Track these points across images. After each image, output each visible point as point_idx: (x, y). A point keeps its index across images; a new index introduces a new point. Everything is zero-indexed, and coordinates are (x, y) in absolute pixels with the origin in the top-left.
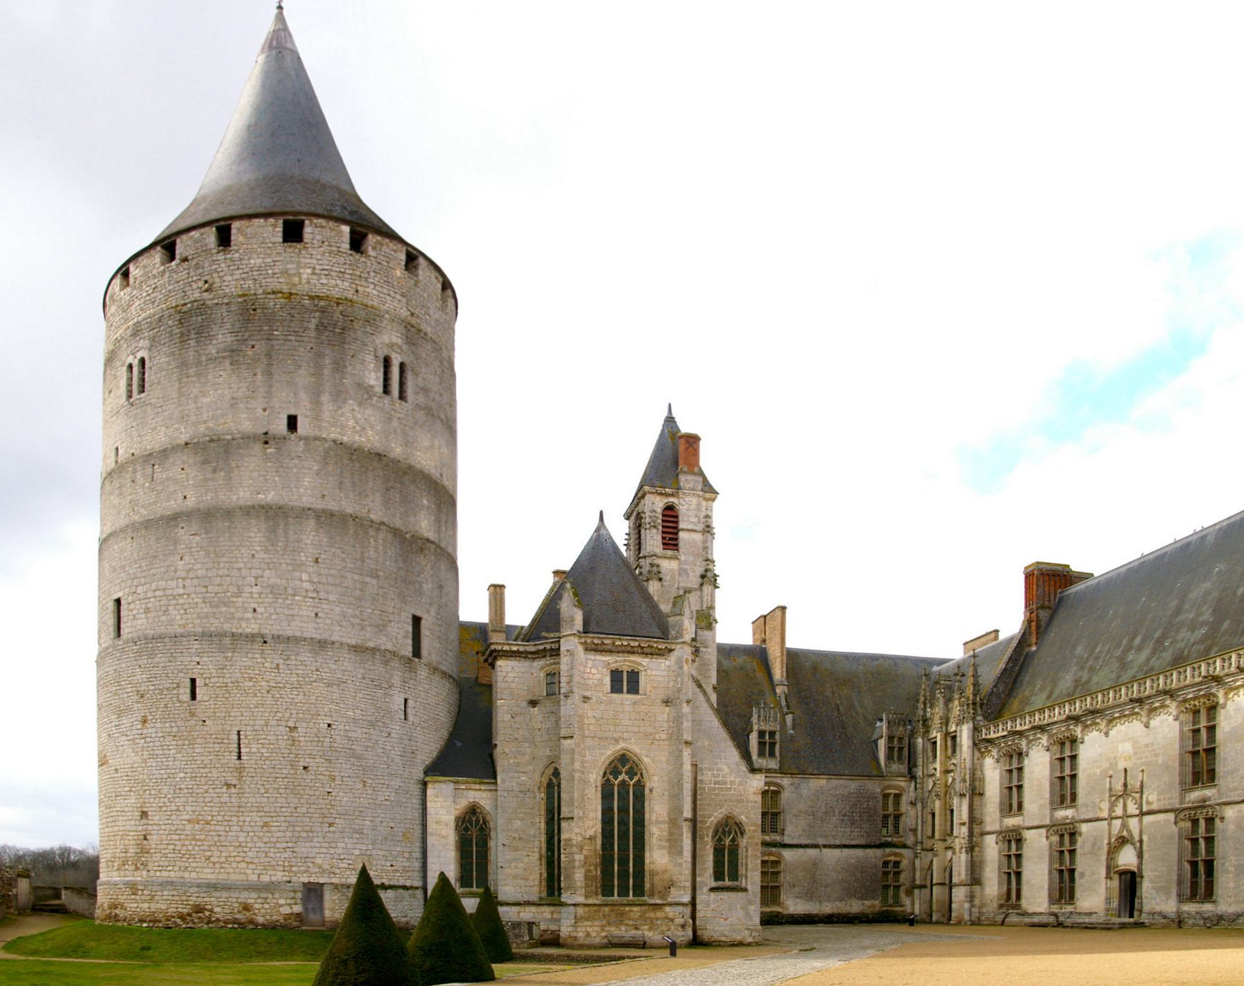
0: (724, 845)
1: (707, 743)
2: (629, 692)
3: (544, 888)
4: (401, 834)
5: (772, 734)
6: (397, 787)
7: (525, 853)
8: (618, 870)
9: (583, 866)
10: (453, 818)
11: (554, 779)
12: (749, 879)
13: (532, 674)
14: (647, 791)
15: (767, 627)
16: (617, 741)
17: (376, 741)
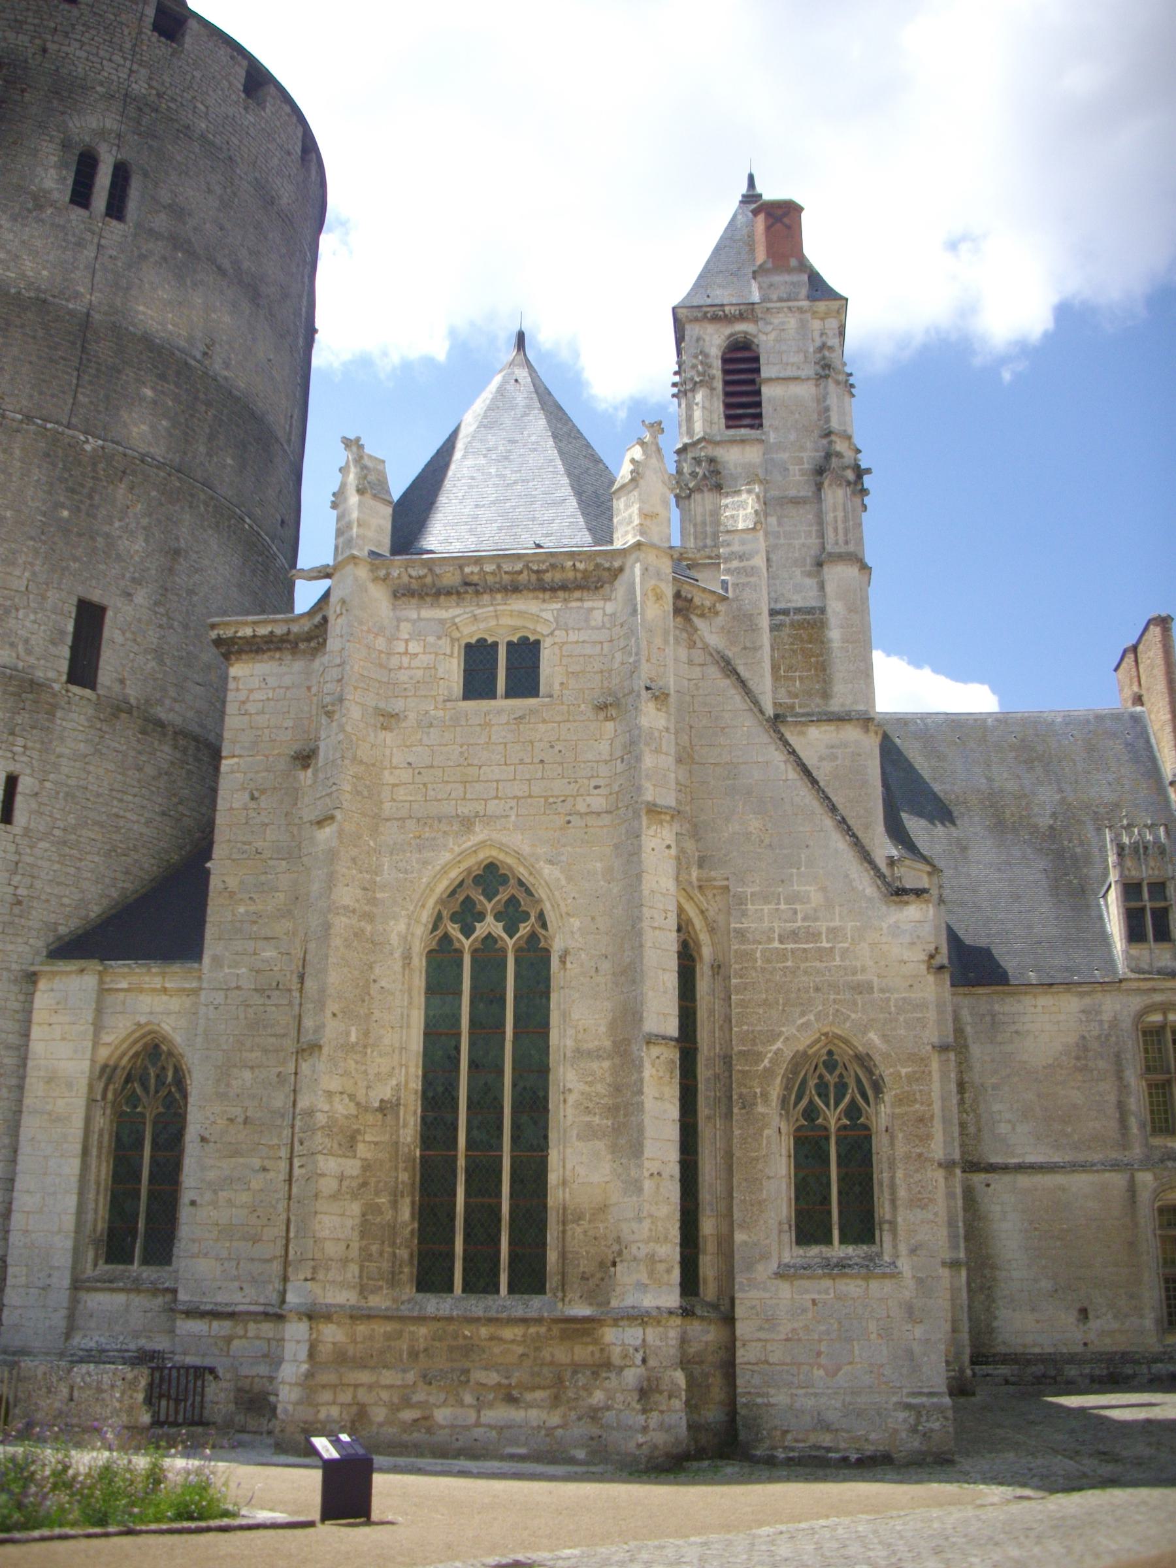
1: (754, 824)
7: (256, 1162)
8: (467, 1205)
9: (355, 1196)
13: (309, 688)
15: (1141, 667)
16: (467, 824)
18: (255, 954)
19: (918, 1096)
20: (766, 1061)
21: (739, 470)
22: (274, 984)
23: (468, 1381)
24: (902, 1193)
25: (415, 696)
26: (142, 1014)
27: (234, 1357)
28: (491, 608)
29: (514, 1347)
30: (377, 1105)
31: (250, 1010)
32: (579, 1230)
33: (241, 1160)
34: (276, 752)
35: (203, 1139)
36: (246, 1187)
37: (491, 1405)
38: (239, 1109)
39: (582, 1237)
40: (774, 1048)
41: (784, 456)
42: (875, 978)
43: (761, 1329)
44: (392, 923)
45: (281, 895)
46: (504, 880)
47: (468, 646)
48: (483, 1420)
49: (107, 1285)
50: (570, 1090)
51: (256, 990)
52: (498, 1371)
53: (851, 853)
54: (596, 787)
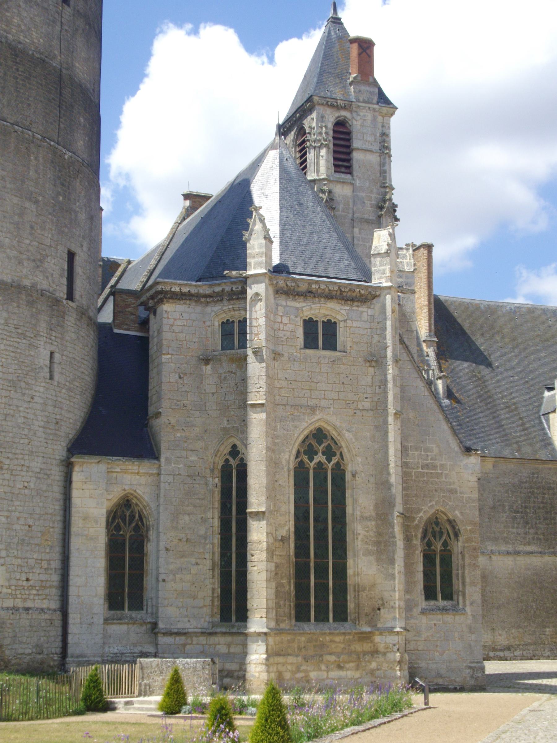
2: (325, 348)
3: (217, 610)
6: (38, 470)
7: (193, 560)
8: (315, 583)
10: (104, 511)
11: (231, 459)
12: (467, 596)
13: (204, 322)
14: (348, 477)
16: (313, 409)
17: (17, 407)
18: (187, 458)
19: (474, 539)
20: (417, 521)
21: (341, 199)
22: (197, 473)
23: (323, 660)
24: (467, 580)
25: (287, 345)
26: (126, 484)
27: (187, 654)
28: (319, 305)
30: (280, 538)
31: (186, 486)
32: (364, 594)
33: (186, 559)
34: (190, 354)
35: (167, 549)
36: (189, 572)
37: (332, 670)
38: (184, 535)
40: (420, 515)
41: (363, 195)
42: (458, 488)
43: (415, 636)
44: (282, 454)
45: (198, 429)
46: (325, 436)
47: (305, 321)
48: (330, 676)
49: (119, 621)
50: (359, 534)
51: (188, 476)
53: (450, 431)
54: (366, 398)
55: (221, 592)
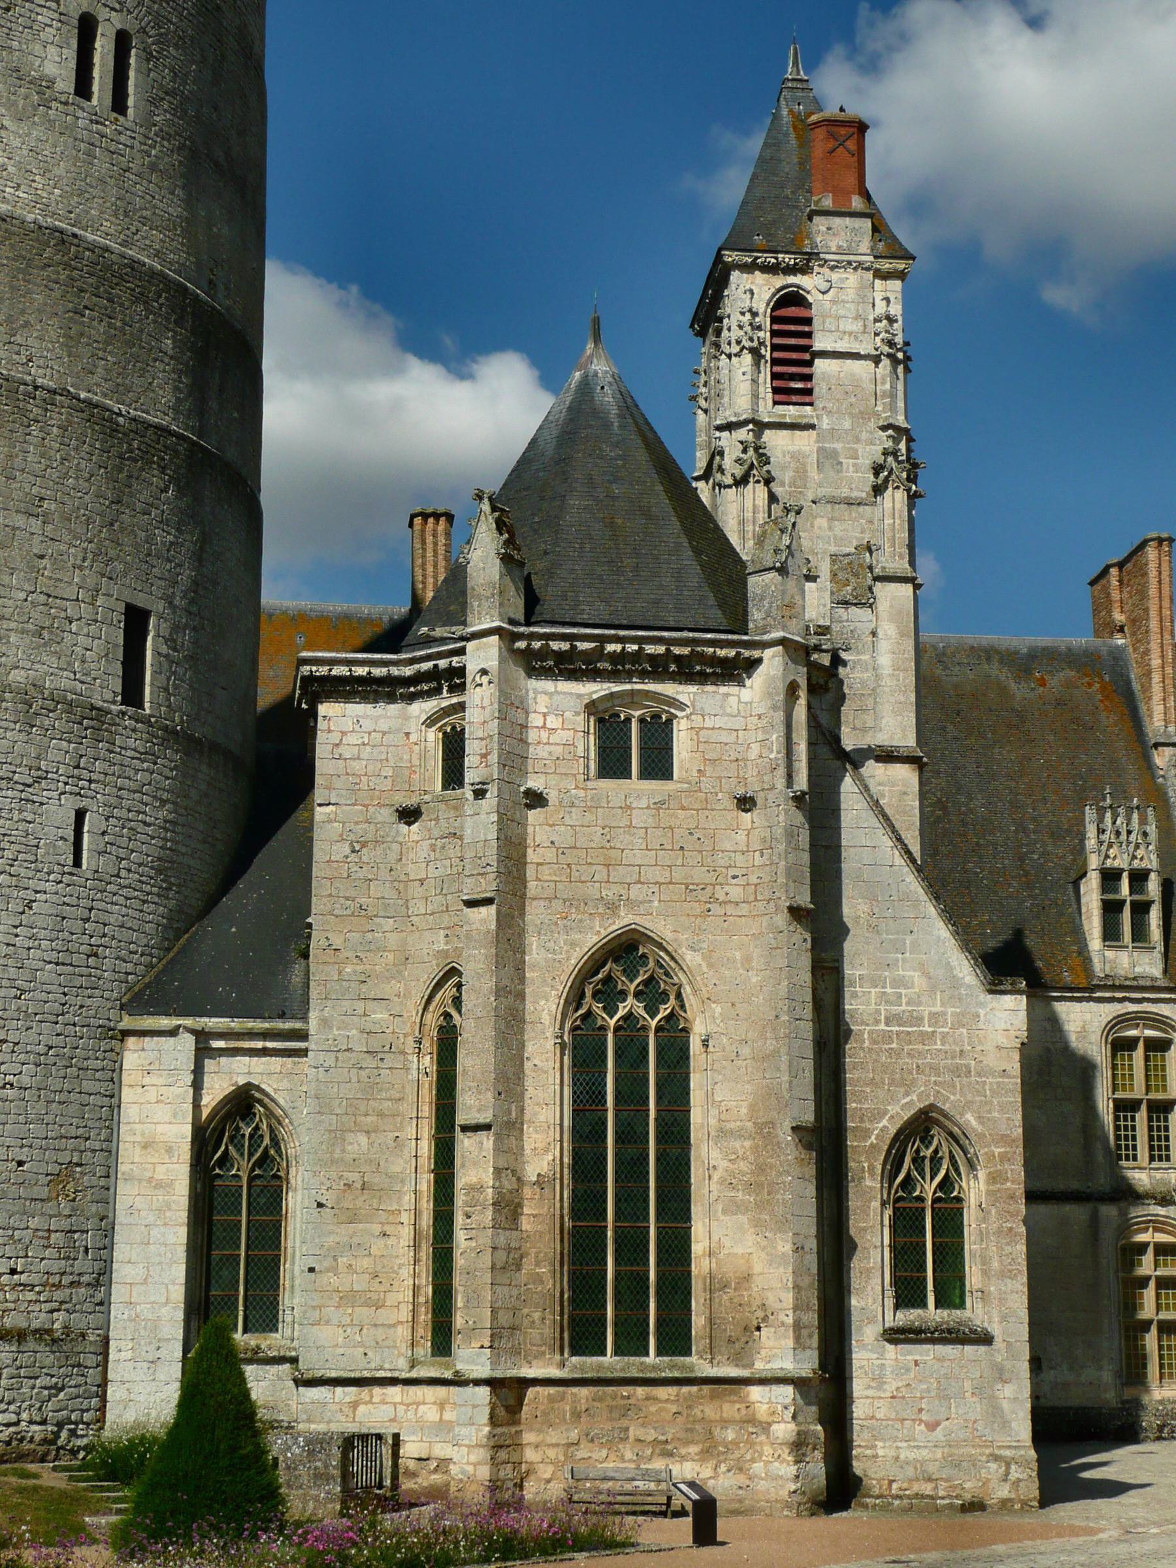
0: (920, 1199)
2: (645, 774)
4: (44, 1180)
5: (1139, 878)
6: (42, 1049)
7: (376, 1228)
13: (407, 734)
16: (612, 908)
18: (365, 1015)
20: (873, 1137)
25: (555, 773)
29: (668, 1406)
30: (535, 1179)
31: (362, 1073)
36: (367, 1252)
39: (728, 1304)
40: (881, 1125)
43: (869, 1387)
44: (542, 1003)
45: (391, 956)
52: (655, 1429)
54: (734, 877)
55: (434, 1292)
